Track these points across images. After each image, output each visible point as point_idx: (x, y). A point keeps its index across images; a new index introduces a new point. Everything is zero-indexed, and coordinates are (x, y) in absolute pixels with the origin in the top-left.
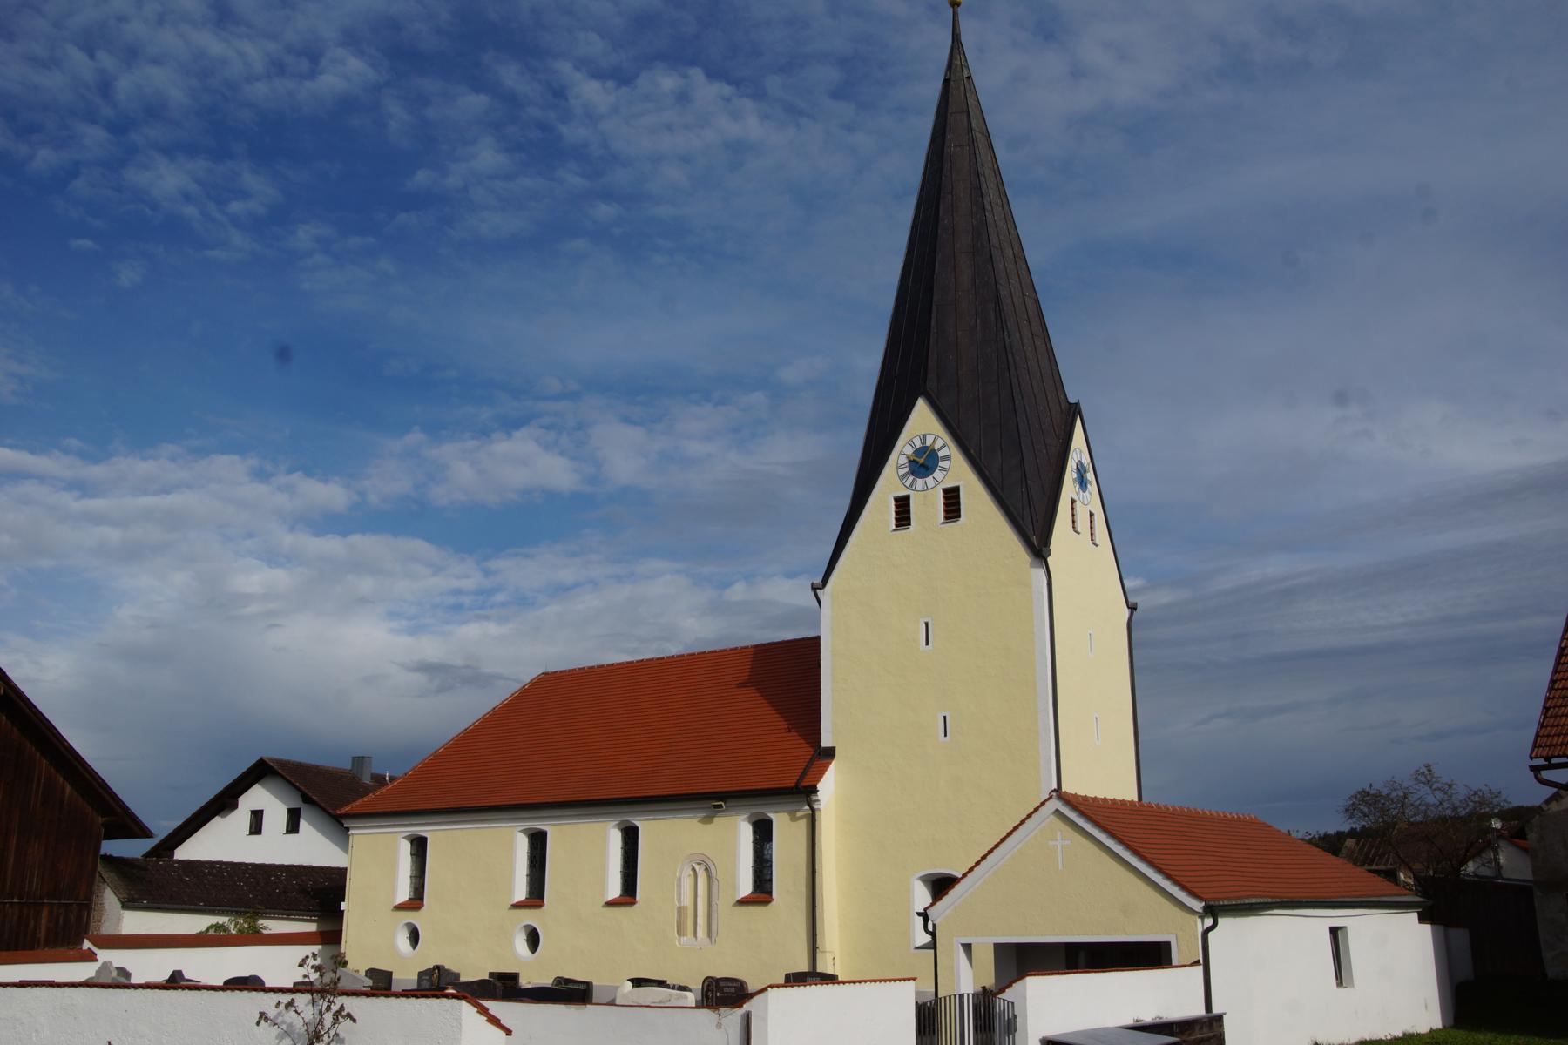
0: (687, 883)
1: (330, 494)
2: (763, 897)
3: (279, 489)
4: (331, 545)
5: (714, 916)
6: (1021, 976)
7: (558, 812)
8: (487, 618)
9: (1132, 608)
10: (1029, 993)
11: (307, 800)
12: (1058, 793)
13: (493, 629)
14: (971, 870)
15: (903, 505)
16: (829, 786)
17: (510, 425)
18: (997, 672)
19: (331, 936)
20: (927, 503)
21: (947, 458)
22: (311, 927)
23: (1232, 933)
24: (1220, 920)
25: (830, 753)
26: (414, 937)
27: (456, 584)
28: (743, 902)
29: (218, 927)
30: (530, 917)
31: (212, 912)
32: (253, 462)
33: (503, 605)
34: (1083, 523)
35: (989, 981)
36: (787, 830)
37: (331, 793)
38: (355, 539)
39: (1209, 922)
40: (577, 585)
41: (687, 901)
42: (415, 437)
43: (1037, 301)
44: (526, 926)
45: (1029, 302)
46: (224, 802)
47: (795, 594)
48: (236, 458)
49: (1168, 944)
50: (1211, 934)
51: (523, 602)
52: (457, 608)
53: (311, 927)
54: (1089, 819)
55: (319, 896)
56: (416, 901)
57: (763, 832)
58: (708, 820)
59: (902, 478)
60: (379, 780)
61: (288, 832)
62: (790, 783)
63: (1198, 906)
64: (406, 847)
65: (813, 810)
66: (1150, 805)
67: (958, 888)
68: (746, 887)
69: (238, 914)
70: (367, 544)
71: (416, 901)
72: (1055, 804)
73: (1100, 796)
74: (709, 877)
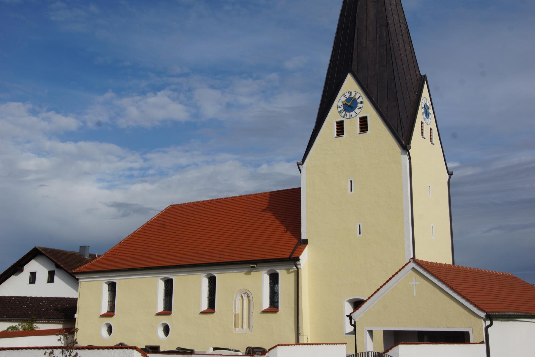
0: (239, 303)
1: (69, 122)
2: (274, 309)
3: (43, 119)
4: (70, 147)
5: (251, 318)
6: (396, 344)
7: (178, 270)
8: (146, 181)
9: (450, 174)
10: (400, 353)
11: (58, 266)
12: (414, 259)
13: (154, 187)
14: (372, 295)
15: (340, 126)
16: (305, 257)
17: (156, 89)
18: (385, 202)
19: (70, 330)
20: (352, 124)
21: (361, 103)
22: (60, 327)
23: (500, 329)
24: (494, 322)
25: (306, 242)
26: (110, 330)
27: (130, 165)
28: (265, 312)
29: (13, 328)
30: (165, 319)
31: (10, 321)
32: (30, 106)
33: (153, 175)
34: (427, 134)
35: (381, 350)
36: (285, 277)
37: (70, 263)
38: (82, 144)
39: (488, 323)
40: (188, 166)
41: (239, 311)
42: (109, 95)
43: (406, 25)
44: (163, 324)
45: (403, 26)
46: (16, 269)
47: (291, 169)
48: (20, 104)
49: (468, 333)
50: (489, 329)
51: (162, 173)
52: (130, 177)
53: (60, 327)
54: (429, 272)
55: (64, 312)
56: (111, 313)
57: (274, 279)
58: (248, 273)
59: (340, 112)
60: (93, 257)
61: (49, 282)
62: (287, 256)
63: (483, 315)
64: (106, 288)
65: (298, 269)
66: (458, 267)
67: (366, 304)
68: (266, 305)
69: (23, 321)
70: (86, 146)
71: (111, 313)
72: (412, 265)
73: (434, 261)
74: (249, 300)
